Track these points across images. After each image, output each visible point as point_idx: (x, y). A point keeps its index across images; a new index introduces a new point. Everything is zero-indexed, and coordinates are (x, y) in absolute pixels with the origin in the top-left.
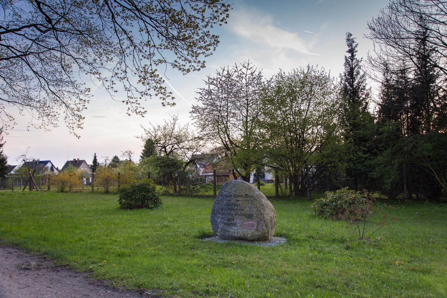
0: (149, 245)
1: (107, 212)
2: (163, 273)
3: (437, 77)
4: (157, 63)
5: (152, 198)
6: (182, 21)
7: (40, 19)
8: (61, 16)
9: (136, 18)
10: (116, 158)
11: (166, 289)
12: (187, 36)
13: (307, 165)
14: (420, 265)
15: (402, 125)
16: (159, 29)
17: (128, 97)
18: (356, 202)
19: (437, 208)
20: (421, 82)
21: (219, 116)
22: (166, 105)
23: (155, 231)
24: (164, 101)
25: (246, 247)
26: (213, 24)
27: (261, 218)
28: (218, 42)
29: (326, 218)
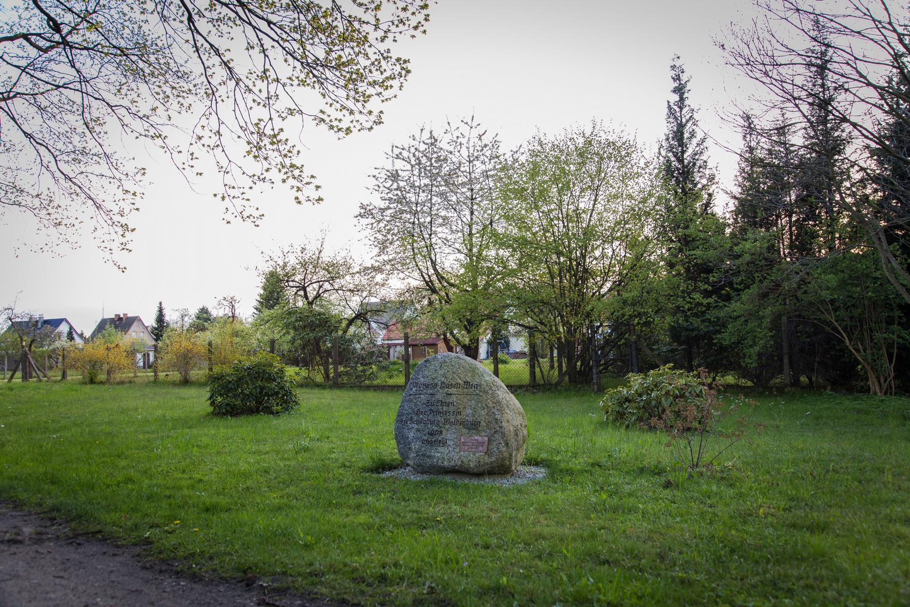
0: (269, 487)
1: (186, 422)
2: (296, 543)
3: (849, 142)
4: (283, 115)
5: (277, 393)
6: (334, 28)
7: (38, 23)
8: (79, 16)
9: (238, 22)
10: (204, 311)
11: (300, 574)
12: (344, 59)
13: (591, 322)
14: (806, 516)
15: (779, 237)
16: (286, 44)
17: (225, 185)
18: (687, 394)
19: (847, 403)
20: (816, 151)
21: (413, 223)
22: (303, 202)
23: (283, 459)
24: (299, 194)
25: (466, 487)
26: (397, 35)
27: (496, 428)
28: (408, 72)
29: (628, 427)
